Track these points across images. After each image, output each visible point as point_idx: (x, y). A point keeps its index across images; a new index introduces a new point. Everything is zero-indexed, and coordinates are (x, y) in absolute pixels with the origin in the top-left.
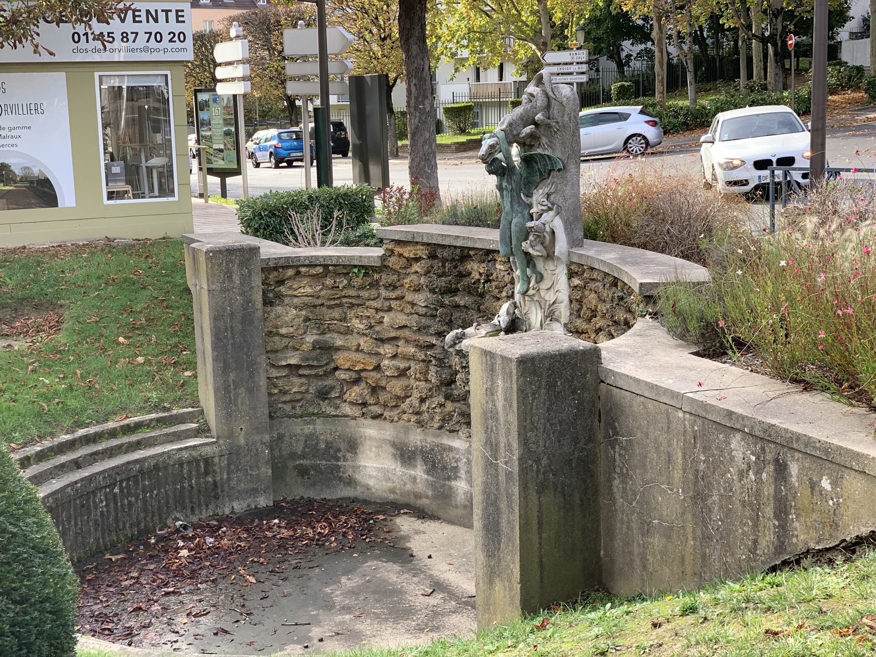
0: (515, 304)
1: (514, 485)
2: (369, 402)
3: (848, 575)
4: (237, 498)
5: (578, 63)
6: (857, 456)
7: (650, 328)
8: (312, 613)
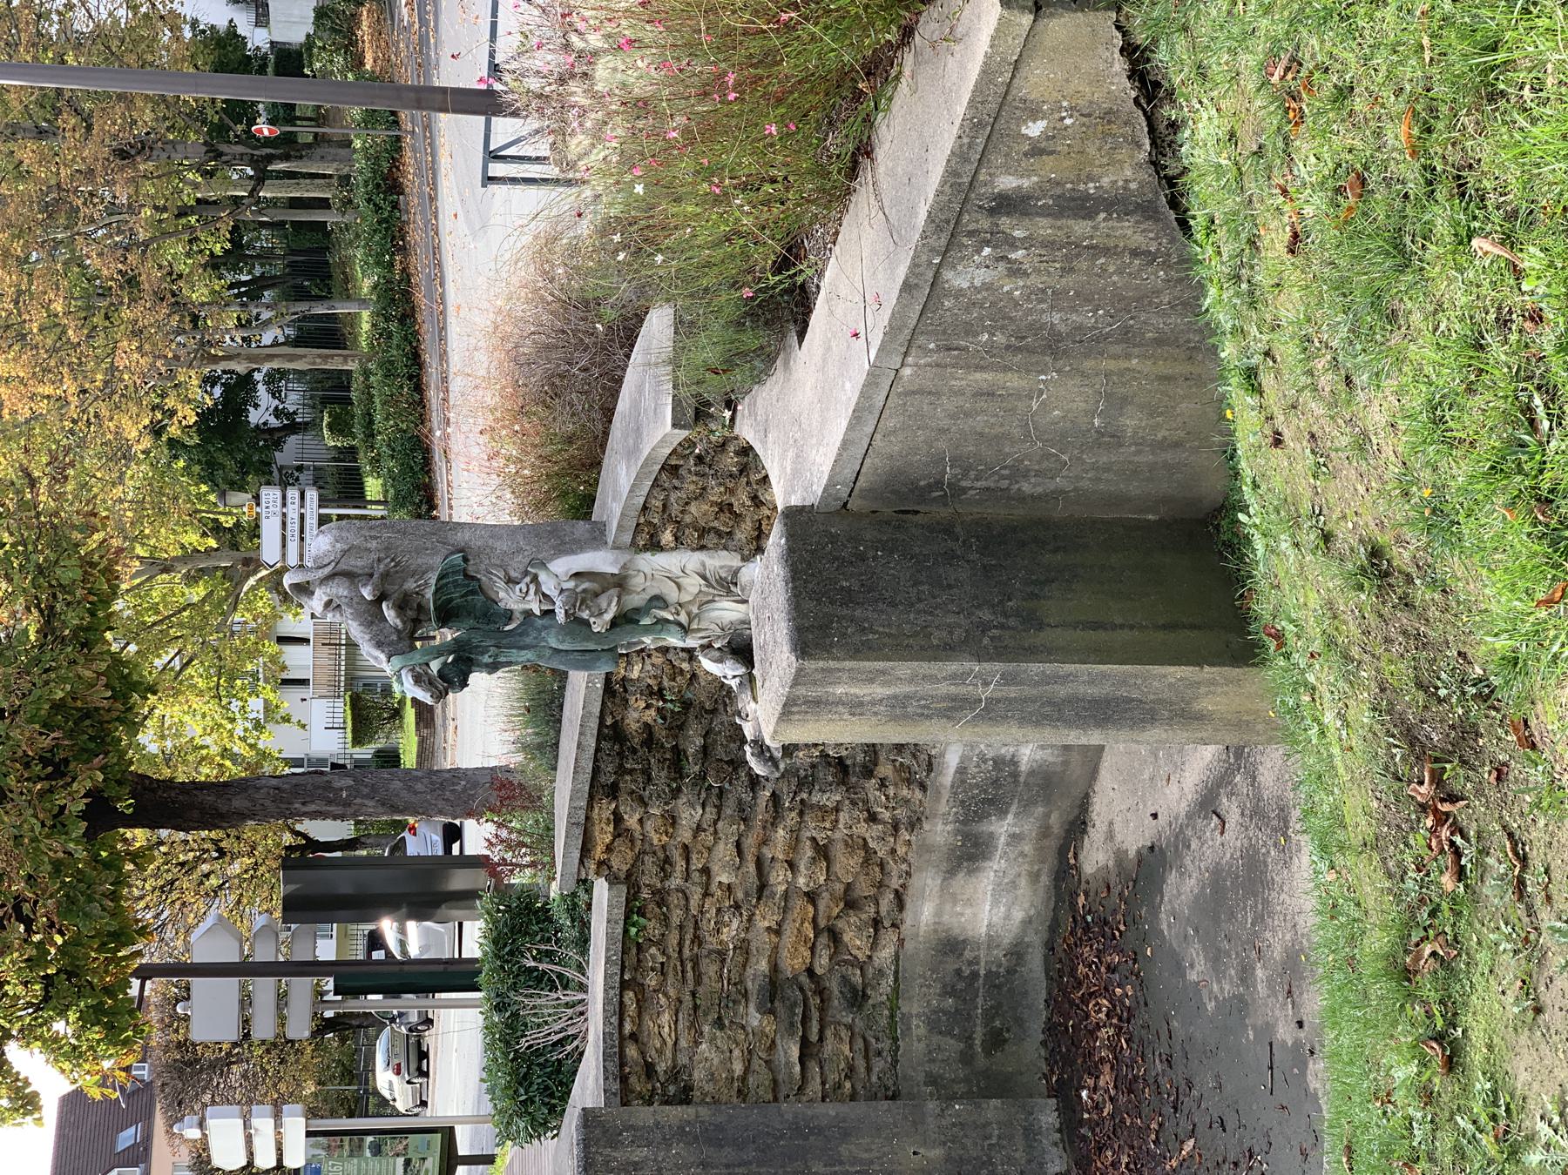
0: (703, 647)
1: (1025, 671)
2: (873, 915)
3: (1195, 100)
4: (1041, 1165)
5: (284, 505)
6: (987, 73)
7: (753, 413)
8: (1251, 1037)
